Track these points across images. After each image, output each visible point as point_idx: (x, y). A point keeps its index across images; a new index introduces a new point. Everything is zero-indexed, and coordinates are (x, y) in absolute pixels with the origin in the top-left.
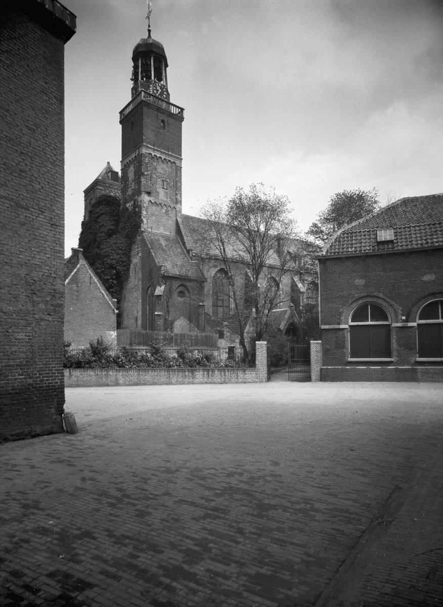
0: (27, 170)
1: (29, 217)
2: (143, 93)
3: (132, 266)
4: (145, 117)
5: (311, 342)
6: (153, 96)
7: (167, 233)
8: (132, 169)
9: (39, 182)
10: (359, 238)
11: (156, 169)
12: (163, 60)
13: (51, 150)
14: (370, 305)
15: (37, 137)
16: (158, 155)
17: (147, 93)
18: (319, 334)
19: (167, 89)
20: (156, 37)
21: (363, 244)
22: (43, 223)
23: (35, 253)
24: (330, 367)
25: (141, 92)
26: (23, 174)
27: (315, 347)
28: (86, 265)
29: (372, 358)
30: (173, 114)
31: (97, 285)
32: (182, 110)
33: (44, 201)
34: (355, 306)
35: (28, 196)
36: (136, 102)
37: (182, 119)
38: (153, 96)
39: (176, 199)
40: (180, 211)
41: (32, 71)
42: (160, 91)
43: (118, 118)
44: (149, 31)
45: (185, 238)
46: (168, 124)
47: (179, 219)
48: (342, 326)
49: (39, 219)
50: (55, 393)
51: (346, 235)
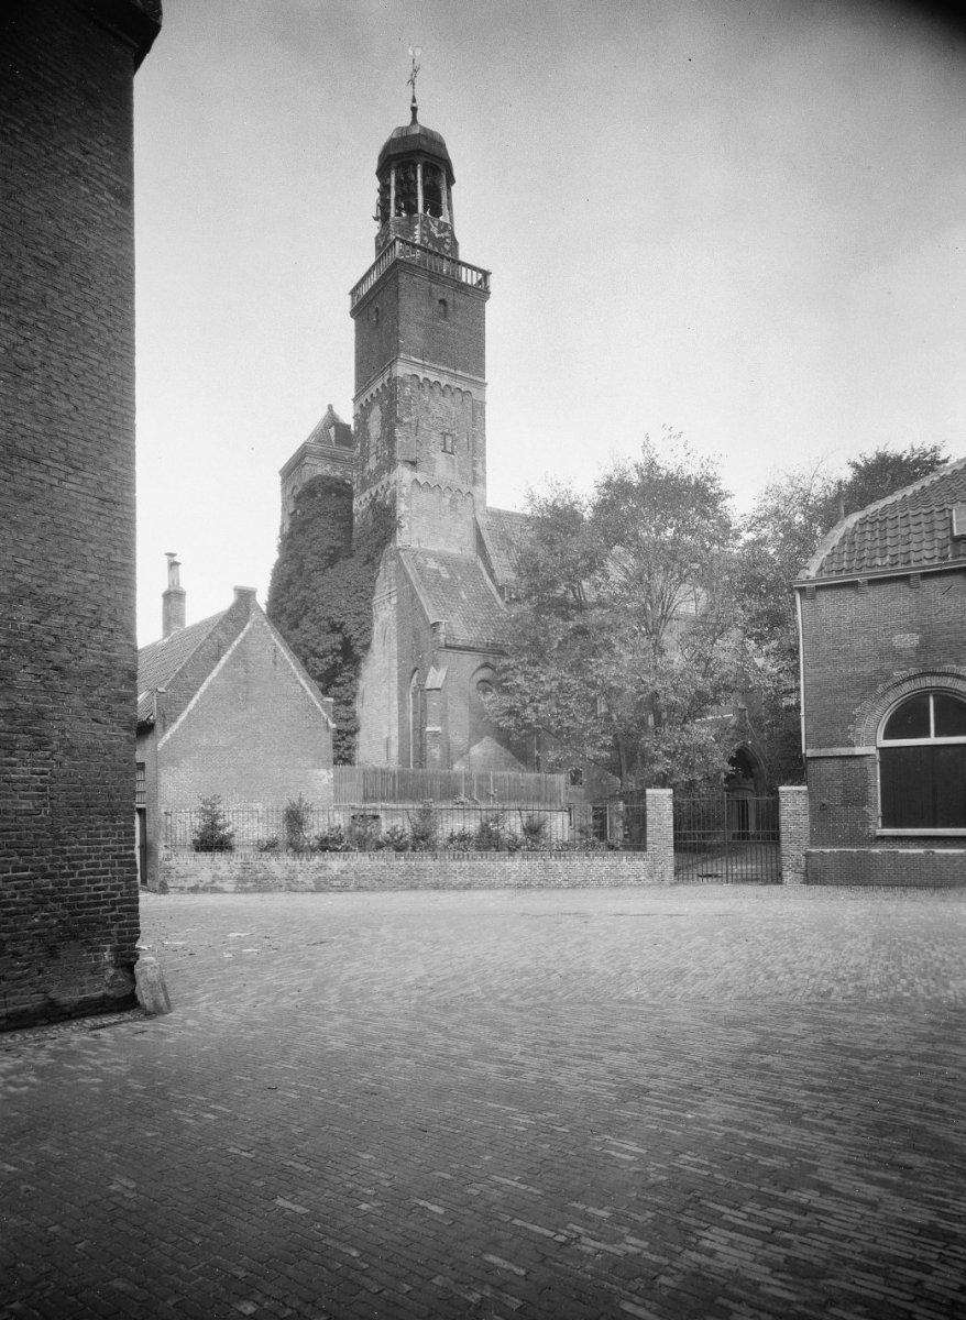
0: (37, 364)
1: (41, 481)
2: (398, 243)
3: (377, 627)
4: (403, 296)
5: (781, 788)
6: (420, 248)
7: (454, 550)
8: (376, 412)
9: (67, 395)
10: (904, 532)
11: (427, 410)
12: (443, 169)
13: (101, 317)
14: (934, 696)
15: (62, 285)
16: (433, 379)
17: (408, 243)
18: (796, 769)
19: (452, 233)
20: (427, 120)
21: (913, 546)
22: (80, 497)
23: (58, 568)
24: (828, 851)
25: (394, 243)
26: (25, 374)
27: (793, 800)
28: (266, 624)
29: (943, 826)
30: (466, 285)
31: (289, 668)
32: (486, 274)
33: (82, 443)
34: (893, 701)
35: (39, 428)
36: (383, 268)
37: (486, 293)
38: (420, 248)
39: (474, 473)
40: (483, 502)
41: (48, 123)
42: (437, 236)
43: (346, 304)
44: (414, 110)
45: (494, 559)
46: (454, 307)
47: (479, 518)
48: (858, 751)
49: (68, 485)
50: (114, 913)
51: (868, 528)
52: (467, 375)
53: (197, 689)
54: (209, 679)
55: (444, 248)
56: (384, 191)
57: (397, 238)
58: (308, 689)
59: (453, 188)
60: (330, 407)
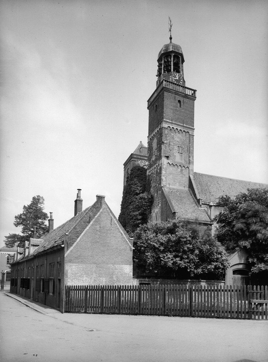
8: (155, 141)
30: (188, 95)
32: (195, 91)
36: (159, 89)
40: (193, 170)
43: (146, 105)
44: (171, 38)
52: (188, 126)
53: (81, 234)
54: (86, 230)
55: (181, 83)
56: (160, 65)
57: (163, 80)
58: (123, 234)
59: (183, 64)
60: (141, 142)
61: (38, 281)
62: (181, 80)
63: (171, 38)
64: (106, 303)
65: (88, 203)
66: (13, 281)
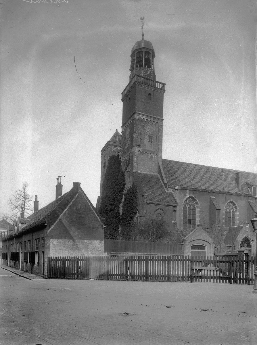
8: (128, 131)
30: (157, 88)
32: (164, 85)
36: (132, 83)
40: (161, 157)
44: (143, 35)
61: (26, 254)
62: (152, 75)
63: (143, 35)
64: (143, 267)
65: (67, 188)
66: (4, 255)
